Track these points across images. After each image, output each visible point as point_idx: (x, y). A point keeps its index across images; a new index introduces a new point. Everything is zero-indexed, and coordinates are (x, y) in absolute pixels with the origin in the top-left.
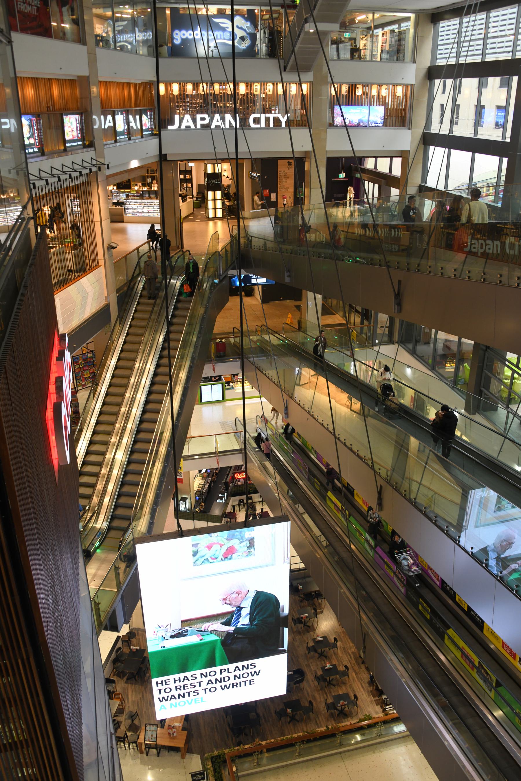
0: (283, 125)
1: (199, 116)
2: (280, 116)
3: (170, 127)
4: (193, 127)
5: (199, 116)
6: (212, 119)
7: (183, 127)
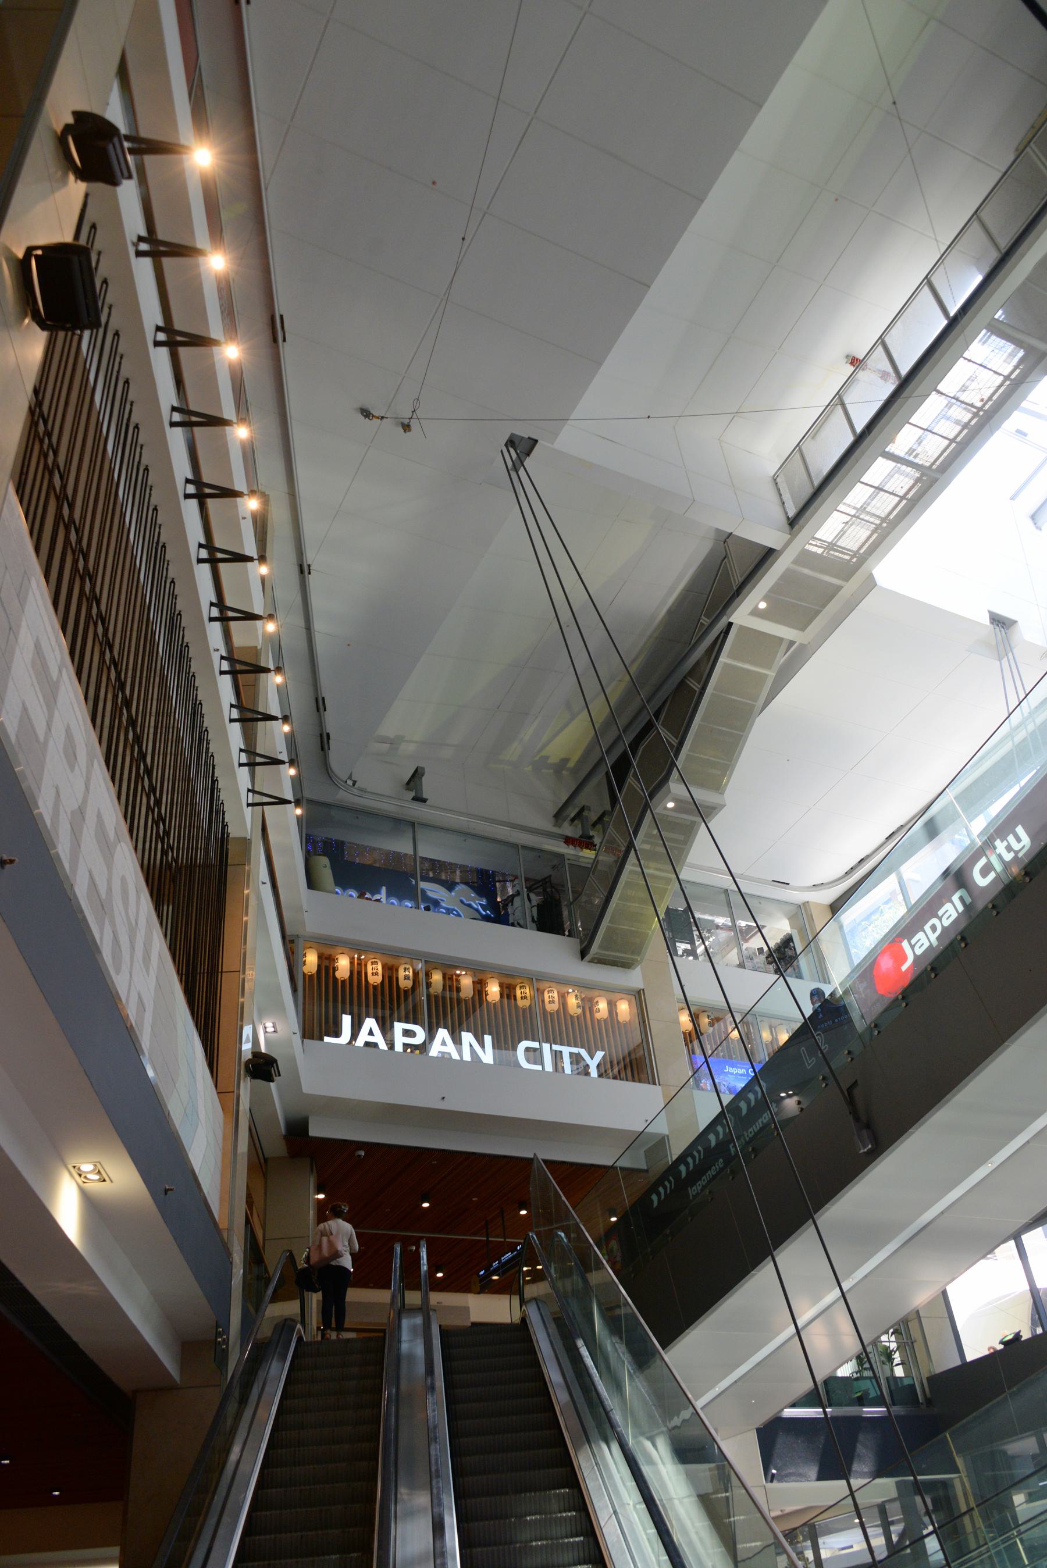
0: (594, 1073)
1: (399, 1027)
2: (583, 1052)
3: (327, 1039)
4: (383, 1046)
5: (399, 1027)
6: (431, 1036)
7: (360, 1042)
